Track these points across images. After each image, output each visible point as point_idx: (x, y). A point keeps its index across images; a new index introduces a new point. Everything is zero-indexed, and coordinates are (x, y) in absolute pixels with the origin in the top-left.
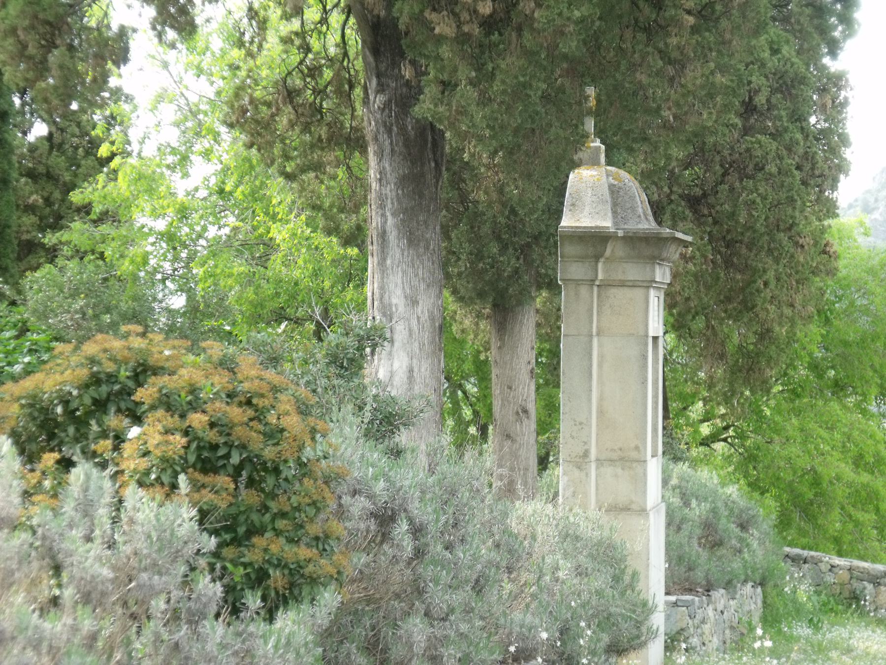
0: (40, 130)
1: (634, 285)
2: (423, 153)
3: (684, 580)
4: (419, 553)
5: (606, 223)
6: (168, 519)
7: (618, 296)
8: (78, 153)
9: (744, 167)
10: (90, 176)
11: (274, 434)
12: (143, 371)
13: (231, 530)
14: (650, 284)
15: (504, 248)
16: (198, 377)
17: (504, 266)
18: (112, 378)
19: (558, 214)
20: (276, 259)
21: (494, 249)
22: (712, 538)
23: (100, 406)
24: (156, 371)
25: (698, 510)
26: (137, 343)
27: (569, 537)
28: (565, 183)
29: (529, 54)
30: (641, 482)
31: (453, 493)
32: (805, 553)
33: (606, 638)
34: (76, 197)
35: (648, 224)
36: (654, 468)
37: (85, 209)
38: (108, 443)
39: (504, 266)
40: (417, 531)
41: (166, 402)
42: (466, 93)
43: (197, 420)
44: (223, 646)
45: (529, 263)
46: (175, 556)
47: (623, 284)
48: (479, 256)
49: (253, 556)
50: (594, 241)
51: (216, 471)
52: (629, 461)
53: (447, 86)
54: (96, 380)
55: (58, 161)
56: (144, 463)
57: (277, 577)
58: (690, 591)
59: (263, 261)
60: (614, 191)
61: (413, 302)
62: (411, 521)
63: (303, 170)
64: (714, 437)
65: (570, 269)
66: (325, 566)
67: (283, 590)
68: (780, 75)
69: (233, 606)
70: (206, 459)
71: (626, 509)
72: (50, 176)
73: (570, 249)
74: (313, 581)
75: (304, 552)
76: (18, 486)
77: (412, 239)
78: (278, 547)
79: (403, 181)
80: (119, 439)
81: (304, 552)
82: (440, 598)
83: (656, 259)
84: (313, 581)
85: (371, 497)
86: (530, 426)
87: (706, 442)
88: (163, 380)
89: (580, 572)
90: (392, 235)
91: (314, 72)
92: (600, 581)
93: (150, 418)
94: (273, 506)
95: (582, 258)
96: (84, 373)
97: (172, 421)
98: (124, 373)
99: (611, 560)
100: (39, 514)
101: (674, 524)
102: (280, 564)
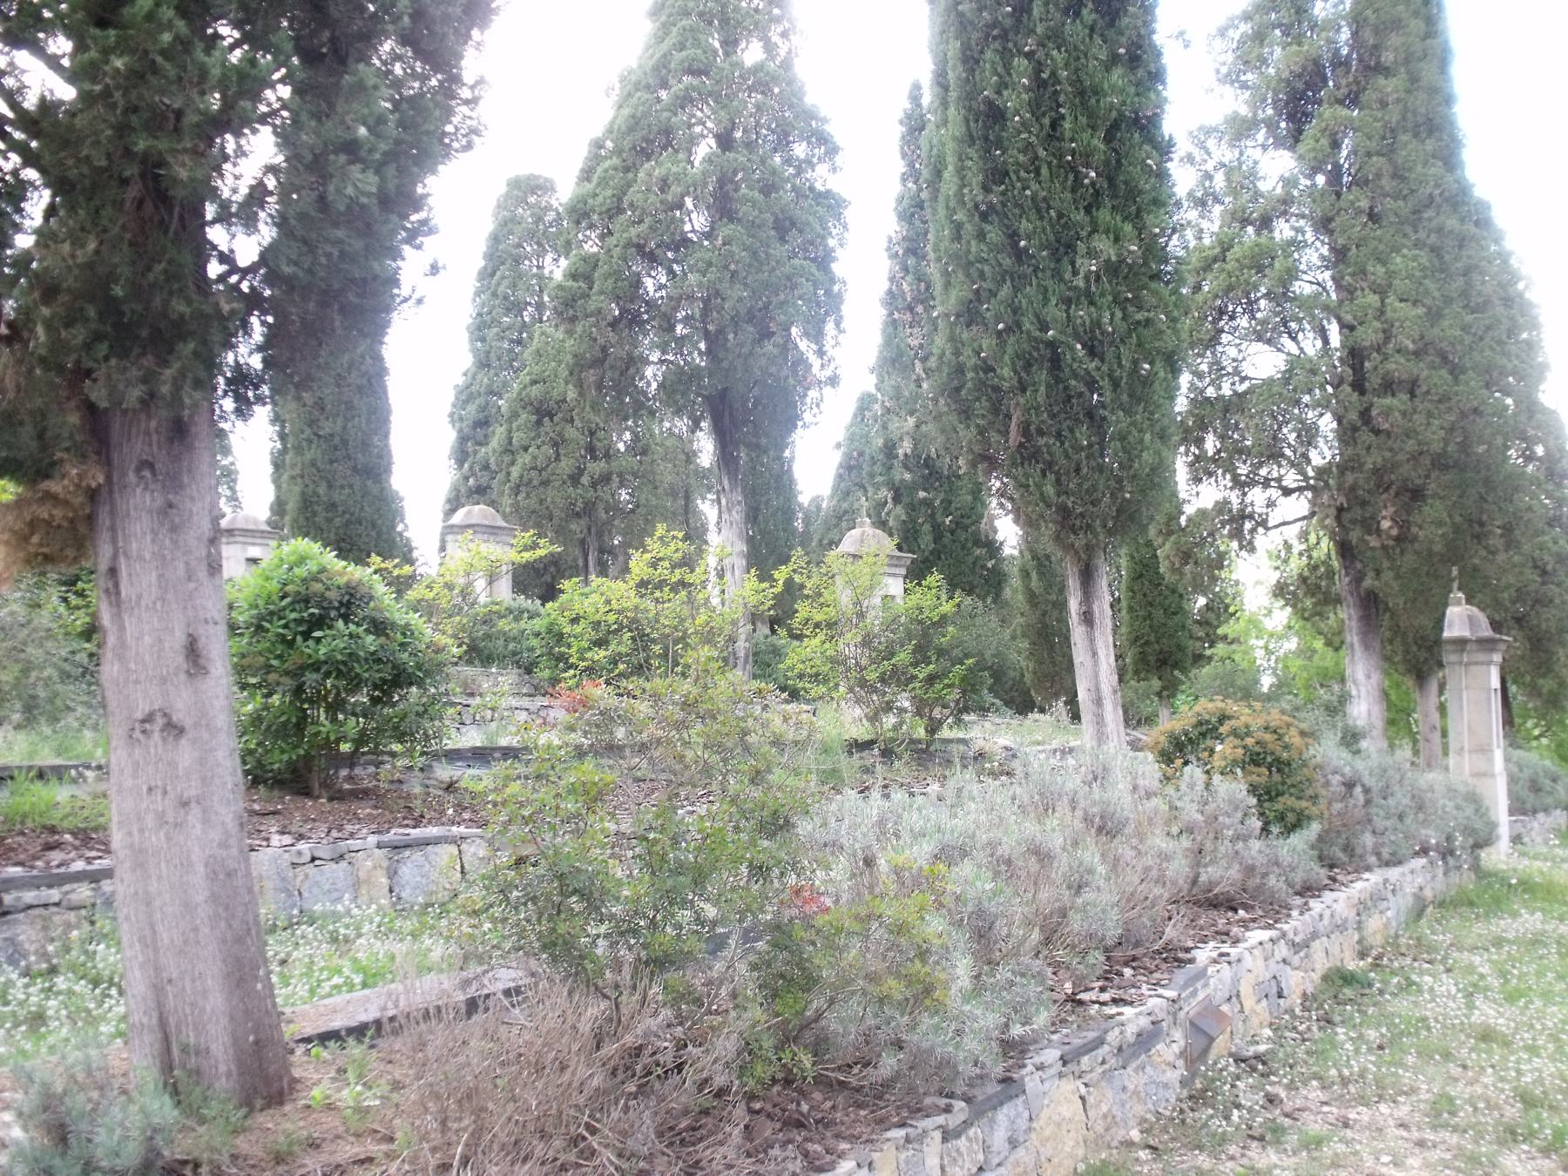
0: (1202, 601)
1: (1482, 663)
2: (1371, 605)
3: (1518, 808)
4: (1368, 802)
5: (1466, 633)
6: (1233, 789)
7: (1474, 668)
8: (1220, 610)
9: (1541, 601)
10: (1227, 621)
11: (1286, 747)
12: (1223, 718)
13: (1265, 795)
14: (1490, 663)
15: (1420, 648)
16: (1249, 720)
17: (1418, 658)
18: (1208, 722)
19: (1442, 630)
20: (1316, 657)
21: (1415, 648)
22: (1535, 787)
23: (1203, 735)
24: (1230, 718)
25: (1527, 773)
26: (1220, 705)
27: (1451, 791)
28: (1444, 614)
29: (1417, 553)
30: (1491, 761)
31: (1385, 771)
32: (415, 833)
33: (1471, 841)
34: (1220, 631)
35: (1487, 632)
36: (1498, 755)
37: (1225, 637)
38: (1206, 754)
39: (1418, 658)
40: (1367, 791)
41: (1234, 733)
42: (1388, 575)
43: (1250, 741)
44: (1260, 852)
45: (1432, 655)
46: (1237, 808)
47: (1476, 663)
48: (1407, 652)
49: (1279, 806)
50: (1461, 643)
51: (1259, 765)
52: (1484, 750)
53: (1378, 572)
54: (1200, 723)
55: (1211, 616)
56: (1223, 763)
57: (1291, 818)
58: (1524, 814)
59: (1310, 658)
60: (1470, 618)
61: (1368, 677)
62: (1363, 786)
63: (1313, 615)
64: (1541, 735)
65: (1449, 657)
66: (1315, 810)
67: (1293, 823)
68: (1558, 554)
69: (1265, 830)
70: (1254, 759)
71: (1484, 775)
72: (1208, 623)
73: (1449, 647)
74: (1309, 818)
75: (1304, 804)
76: (1159, 775)
77: (1367, 646)
78: (1290, 801)
79: (1361, 619)
80: (1212, 751)
81: (1304, 804)
82: (1380, 823)
83: (1492, 650)
84: (1309, 818)
85: (1343, 775)
86: (1438, 734)
87: (1537, 738)
88: (1233, 722)
89: (1458, 808)
90: (1357, 645)
91: (1316, 568)
92: (1469, 811)
93: (1227, 741)
94: (1289, 782)
95: (1455, 652)
96: (1194, 720)
97: (1237, 742)
98: (1214, 720)
99: (1473, 799)
100: (1170, 790)
101: (1512, 780)
102: (1293, 810)
